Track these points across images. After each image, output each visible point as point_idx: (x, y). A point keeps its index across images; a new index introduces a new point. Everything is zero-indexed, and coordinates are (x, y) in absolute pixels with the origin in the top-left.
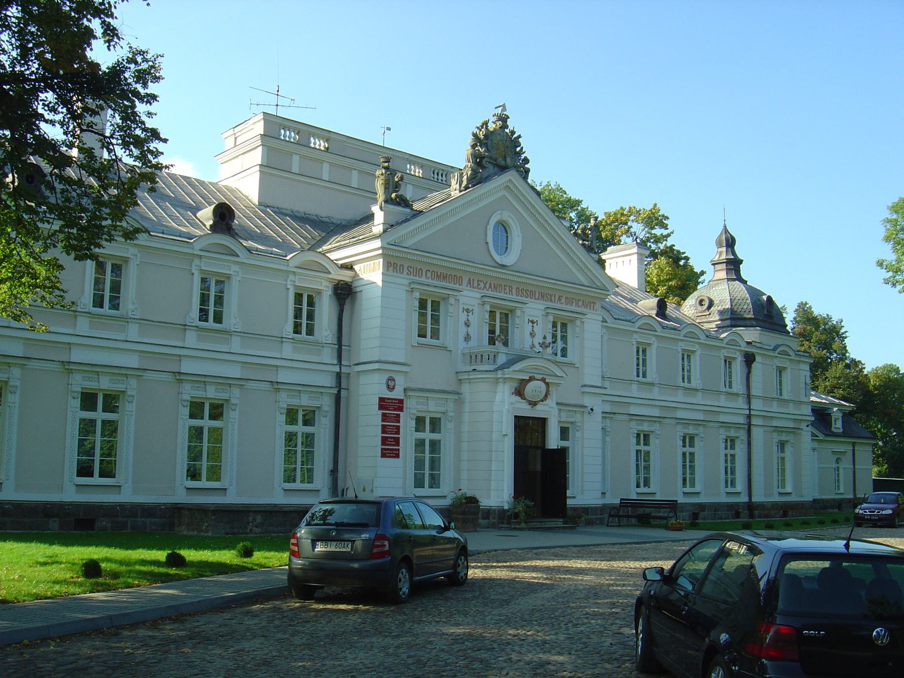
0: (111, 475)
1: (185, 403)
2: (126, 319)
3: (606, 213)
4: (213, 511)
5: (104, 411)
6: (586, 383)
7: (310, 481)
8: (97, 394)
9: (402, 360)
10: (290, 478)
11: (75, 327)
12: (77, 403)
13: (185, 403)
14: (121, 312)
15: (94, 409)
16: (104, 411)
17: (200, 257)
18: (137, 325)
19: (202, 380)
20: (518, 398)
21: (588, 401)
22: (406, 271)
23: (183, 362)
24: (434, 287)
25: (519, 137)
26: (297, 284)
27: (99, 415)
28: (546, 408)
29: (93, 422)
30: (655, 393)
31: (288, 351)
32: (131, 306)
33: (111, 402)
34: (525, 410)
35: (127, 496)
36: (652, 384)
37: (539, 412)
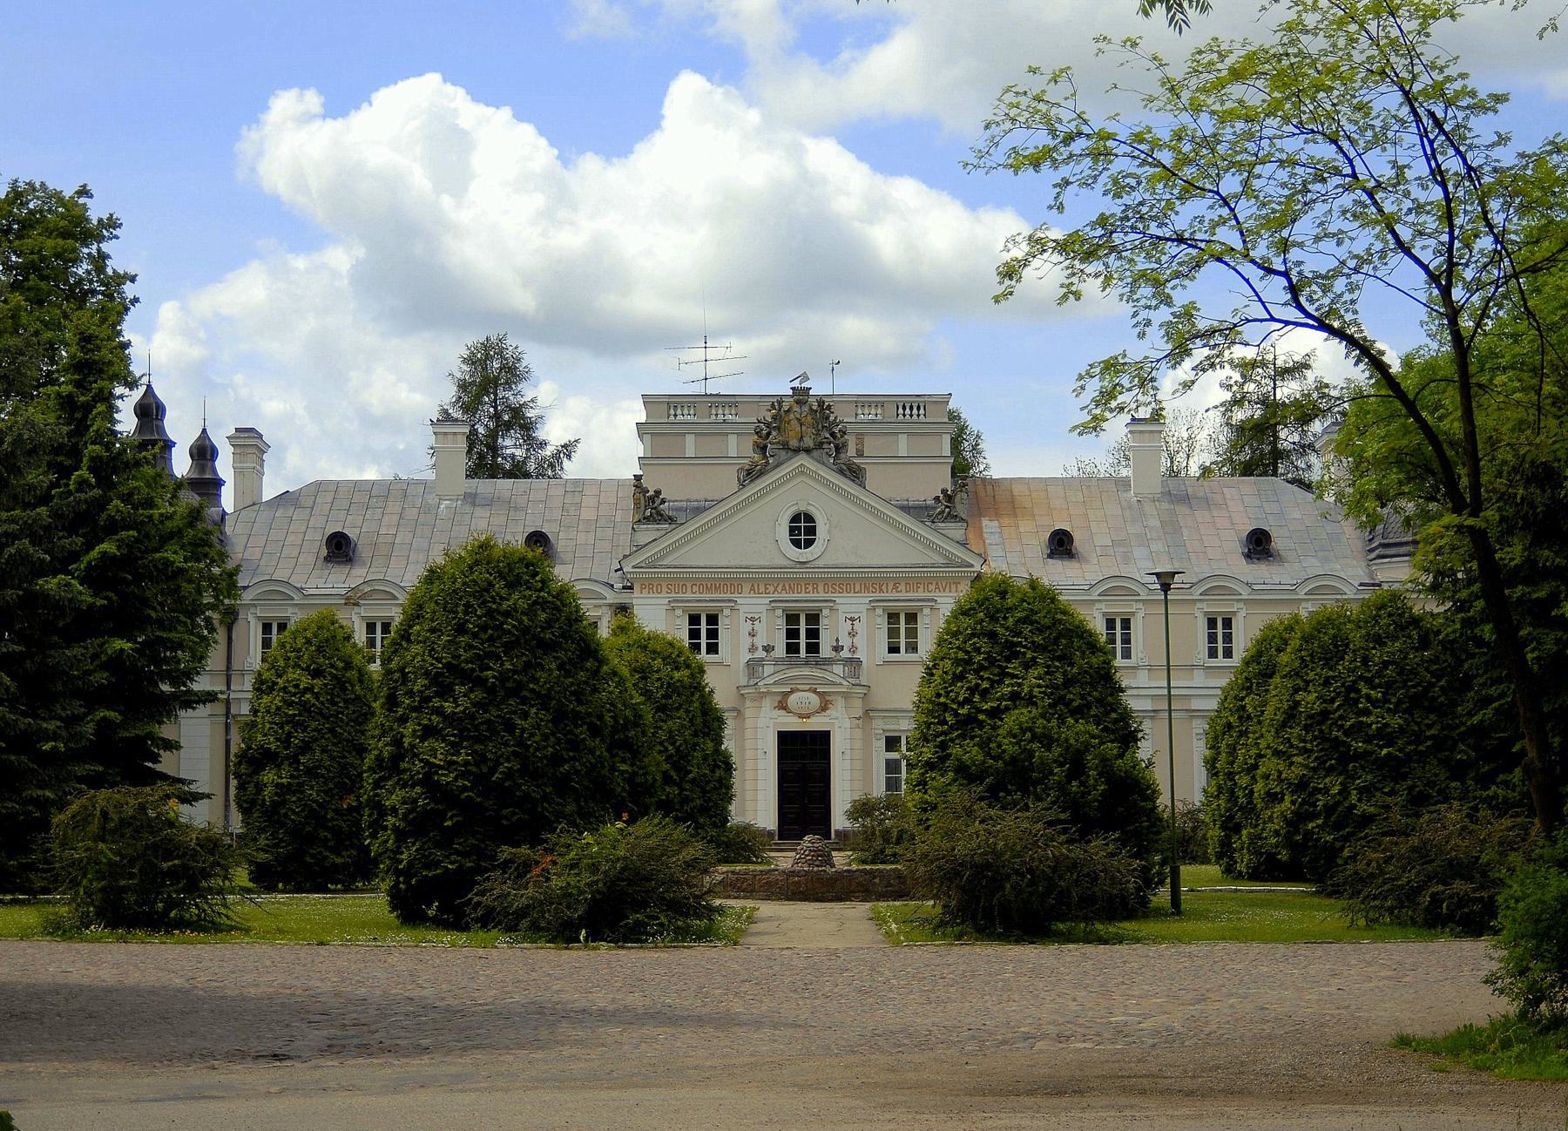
20: (782, 712)
28: (827, 720)
34: (793, 724)
37: (815, 724)
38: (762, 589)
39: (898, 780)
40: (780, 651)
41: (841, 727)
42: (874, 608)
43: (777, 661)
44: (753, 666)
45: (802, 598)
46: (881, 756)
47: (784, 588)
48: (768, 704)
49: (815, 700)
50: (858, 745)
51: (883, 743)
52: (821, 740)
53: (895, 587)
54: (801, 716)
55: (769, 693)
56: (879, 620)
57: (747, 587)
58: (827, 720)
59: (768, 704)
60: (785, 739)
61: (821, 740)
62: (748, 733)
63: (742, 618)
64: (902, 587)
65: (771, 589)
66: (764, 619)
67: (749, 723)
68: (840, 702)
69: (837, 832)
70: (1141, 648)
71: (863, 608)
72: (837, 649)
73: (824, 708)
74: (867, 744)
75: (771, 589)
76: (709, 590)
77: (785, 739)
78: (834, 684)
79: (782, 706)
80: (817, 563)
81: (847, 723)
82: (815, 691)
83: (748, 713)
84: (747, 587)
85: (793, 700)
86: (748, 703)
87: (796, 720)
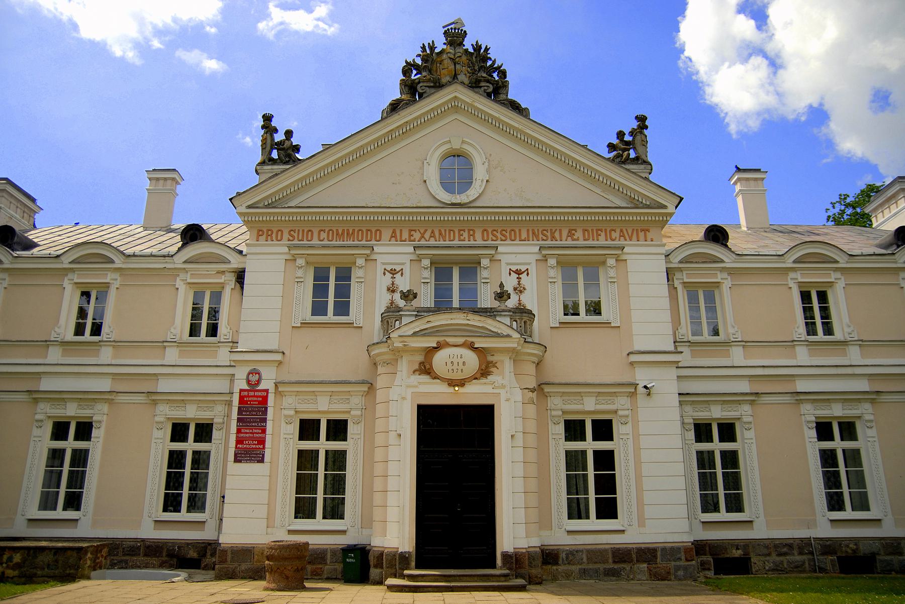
0: (739, 509)
1: (810, 425)
2: (727, 343)
3: (636, 118)
4: (97, 550)
5: (595, 439)
6: (637, 348)
7: (739, 509)
8: (831, 423)
9: (274, 347)
10: (835, 503)
11: (795, 357)
12: (813, 433)
13: (810, 425)
14: (722, 337)
15: (710, 439)
16: (595, 439)
17: (680, 270)
18: (805, 347)
19: (59, 398)
20: (425, 378)
21: (642, 377)
22: (286, 236)
23: (797, 382)
24: (333, 254)
25: (487, 49)
26: (686, 280)
27: (322, 445)
28: (488, 389)
29: (62, 452)
30: (854, 355)
31: (802, 355)
32: (731, 331)
33: (338, 429)
34: (439, 394)
35: (760, 531)
36: (844, 343)
37: (473, 394)
38: (405, 235)
39: (837, 474)
40: (426, 299)
41: (507, 398)
42: (545, 259)
43: (420, 313)
44: (391, 315)
45: (456, 246)
46: (559, 446)
47: (433, 235)
48: (405, 366)
49: (472, 360)
50: (532, 426)
51: (561, 429)
52: (482, 418)
53: (571, 234)
54: (452, 383)
55: (406, 350)
56: (552, 273)
57: (386, 234)
58: (488, 389)
59: (405, 366)
60: (428, 416)
61: (482, 418)
62: (380, 410)
63: (380, 269)
64: (579, 234)
65: (417, 235)
66: (407, 272)
67: (380, 395)
68: (507, 365)
69: (505, 556)
70: (846, 320)
71: (532, 259)
72: (502, 295)
73: (484, 372)
74: (542, 434)
75: (417, 235)
76: (340, 236)
77: (428, 416)
78: (498, 335)
79: (425, 369)
80: (472, 205)
81: (518, 395)
82: (471, 347)
83: (380, 382)
84: (386, 234)
85: (440, 359)
86: (380, 370)
87: (443, 388)
